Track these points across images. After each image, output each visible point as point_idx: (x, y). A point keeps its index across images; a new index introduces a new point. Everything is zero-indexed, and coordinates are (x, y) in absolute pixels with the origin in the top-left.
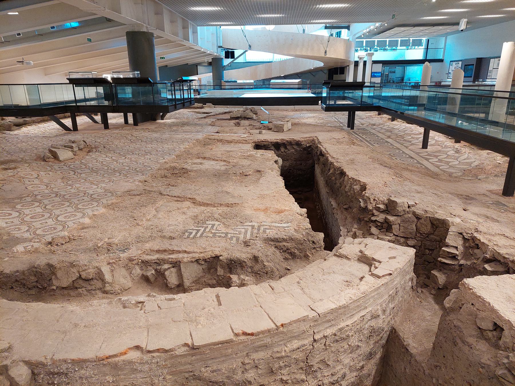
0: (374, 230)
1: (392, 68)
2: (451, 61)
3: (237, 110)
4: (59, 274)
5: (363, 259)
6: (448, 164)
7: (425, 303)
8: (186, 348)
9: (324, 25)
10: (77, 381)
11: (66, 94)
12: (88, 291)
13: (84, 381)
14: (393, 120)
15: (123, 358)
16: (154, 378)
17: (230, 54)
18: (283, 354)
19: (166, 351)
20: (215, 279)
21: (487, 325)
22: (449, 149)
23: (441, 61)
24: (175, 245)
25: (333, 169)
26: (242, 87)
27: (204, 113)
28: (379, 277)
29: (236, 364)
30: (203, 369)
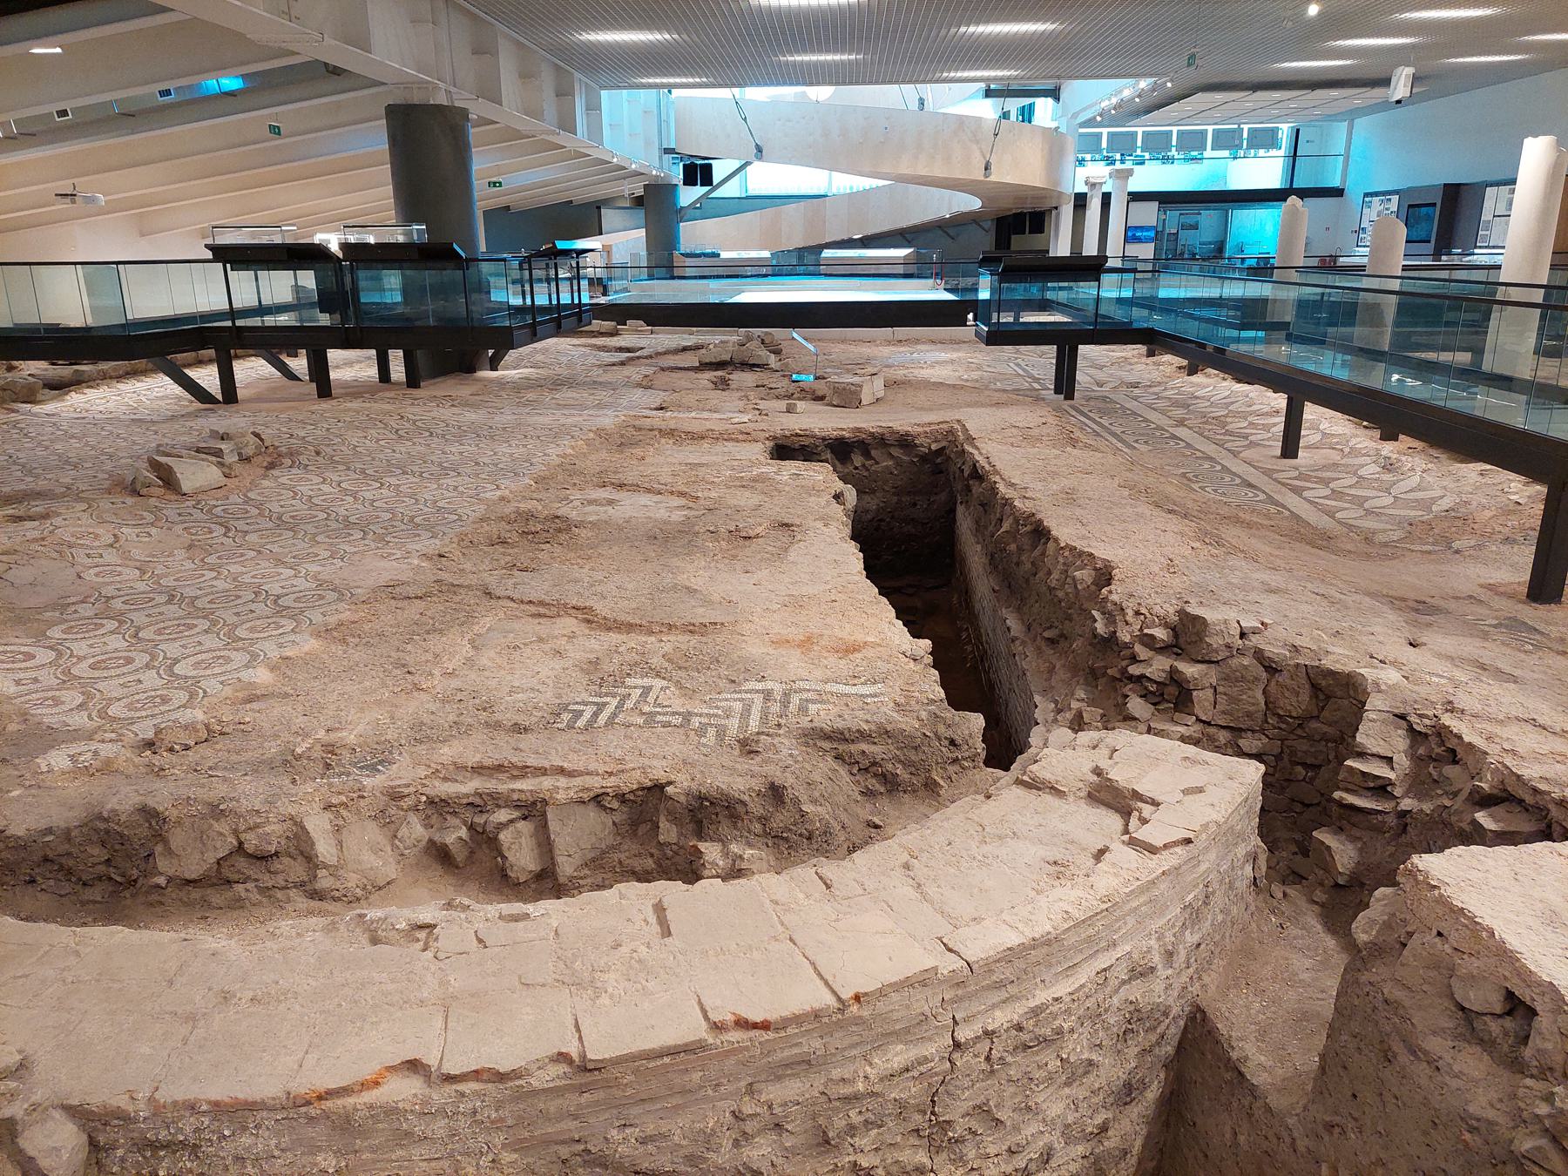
0: (1136, 705)
1: (1190, 214)
2: (1366, 195)
4: (177, 839)
5: (1102, 796)
7: (1294, 931)
8: (562, 1068)
9: (983, 85)
11: (204, 293)
12: (264, 891)
14: (1192, 371)
15: (368, 1097)
17: (698, 173)
18: (860, 1086)
19: (500, 1077)
20: (652, 855)
21: (1483, 998)
23: (1338, 192)
24: (530, 751)
25: (1011, 520)
26: (737, 272)
27: (621, 349)
28: (1152, 850)
29: (714, 1117)
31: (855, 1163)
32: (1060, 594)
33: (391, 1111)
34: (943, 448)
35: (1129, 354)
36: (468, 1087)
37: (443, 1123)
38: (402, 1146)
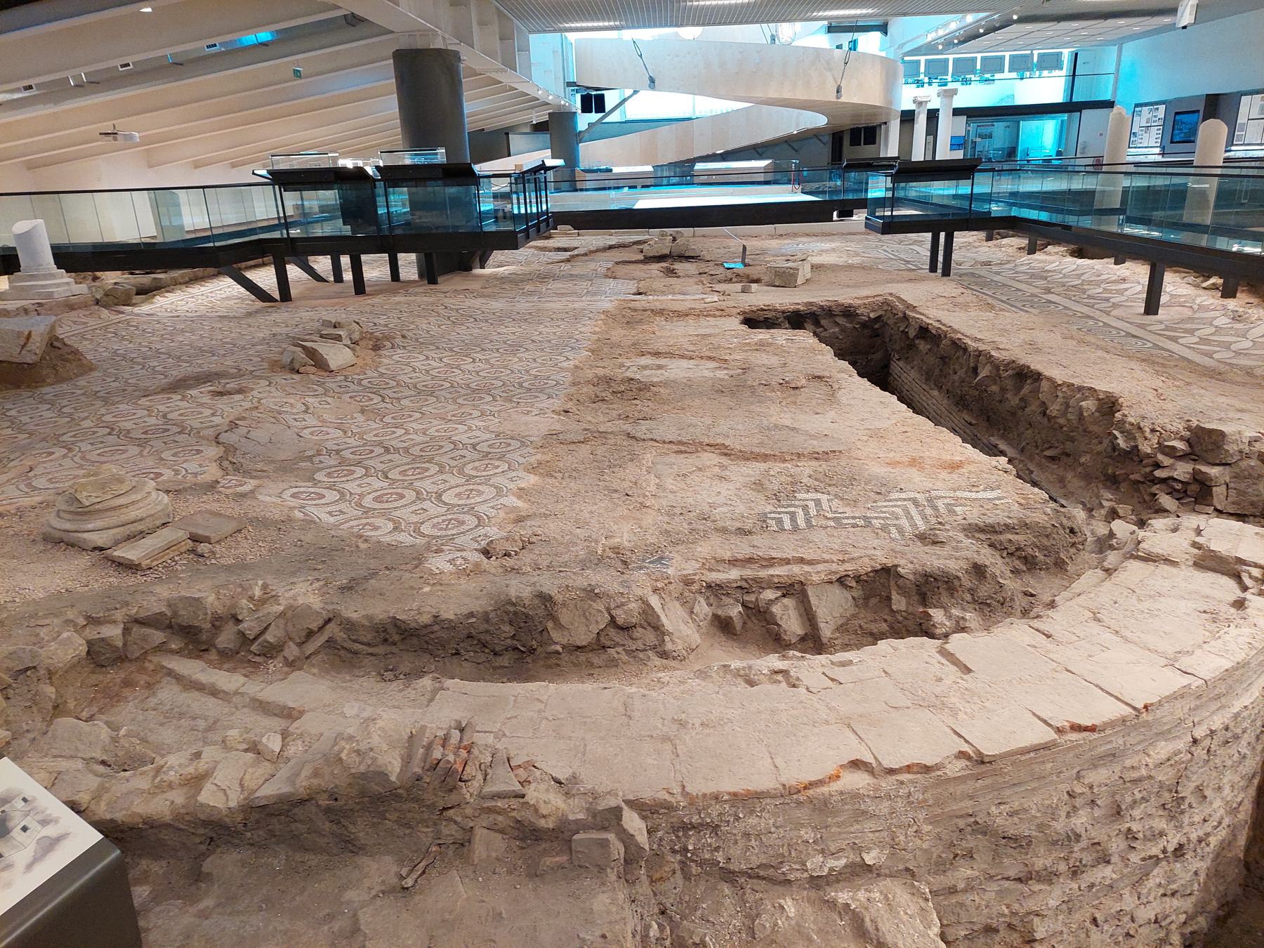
0: (1166, 501)
1: (986, 126)
2: (1137, 105)
3: (656, 239)
4: (565, 617)
5: (1208, 563)
6: (1228, 348)
8: (963, 763)
9: (826, 23)
10: (736, 842)
11: (263, 208)
12: (629, 652)
13: (753, 843)
14: (1032, 250)
16: (898, 832)
17: (593, 102)
18: (1144, 772)
19: (927, 769)
20: (886, 621)
22: (1212, 314)
23: (1109, 104)
24: (763, 545)
25: (988, 367)
26: (621, 182)
27: (559, 249)
29: (1056, 795)
30: (993, 808)
31: (1129, 829)
32: (1062, 421)
33: (856, 796)
34: (880, 317)
35: (971, 240)
36: (905, 777)
37: (887, 804)
38: (857, 821)
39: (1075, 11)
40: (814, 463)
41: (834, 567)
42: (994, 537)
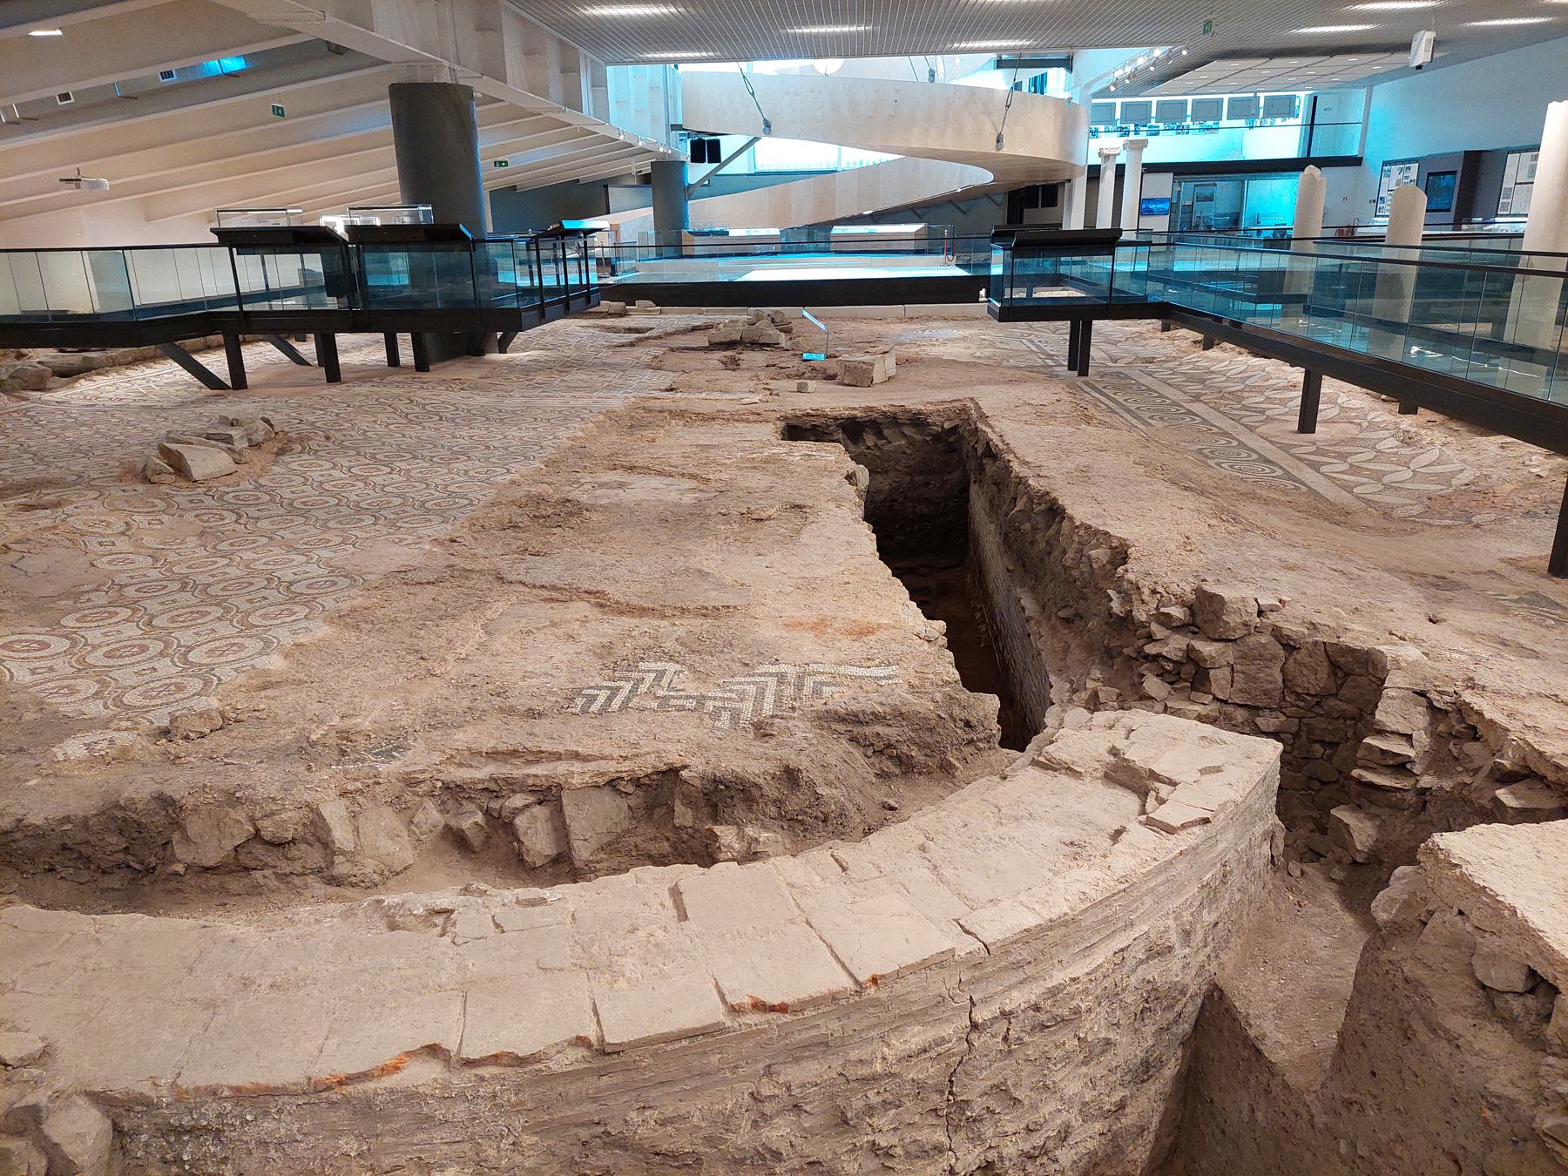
0: (1153, 685)
1: (1206, 185)
2: (1385, 163)
4: (194, 826)
5: (1120, 776)
6: (1380, 480)
8: (582, 1052)
9: (994, 56)
10: (250, 1153)
11: (211, 278)
12: (282, 877)
14: (1208, 345)
15: (388, 1082)
17: (705, 149)
18: (878, 1067)
19: (519, 1061)
20: (668, 839)
22: (1381, 434)
23: (1356, 161)
24: (544, 736)
25: (1025, 499)
26: (745, 250)
27: (630, 330)
28: (1170, 830)
29: (733, 1098)
30: (633, 1115)
33: (412, 1096)
34: (956, 427)
39: (1282, 46)
40: (700, 621)
41: (604, 766)
42: (856, 730)
